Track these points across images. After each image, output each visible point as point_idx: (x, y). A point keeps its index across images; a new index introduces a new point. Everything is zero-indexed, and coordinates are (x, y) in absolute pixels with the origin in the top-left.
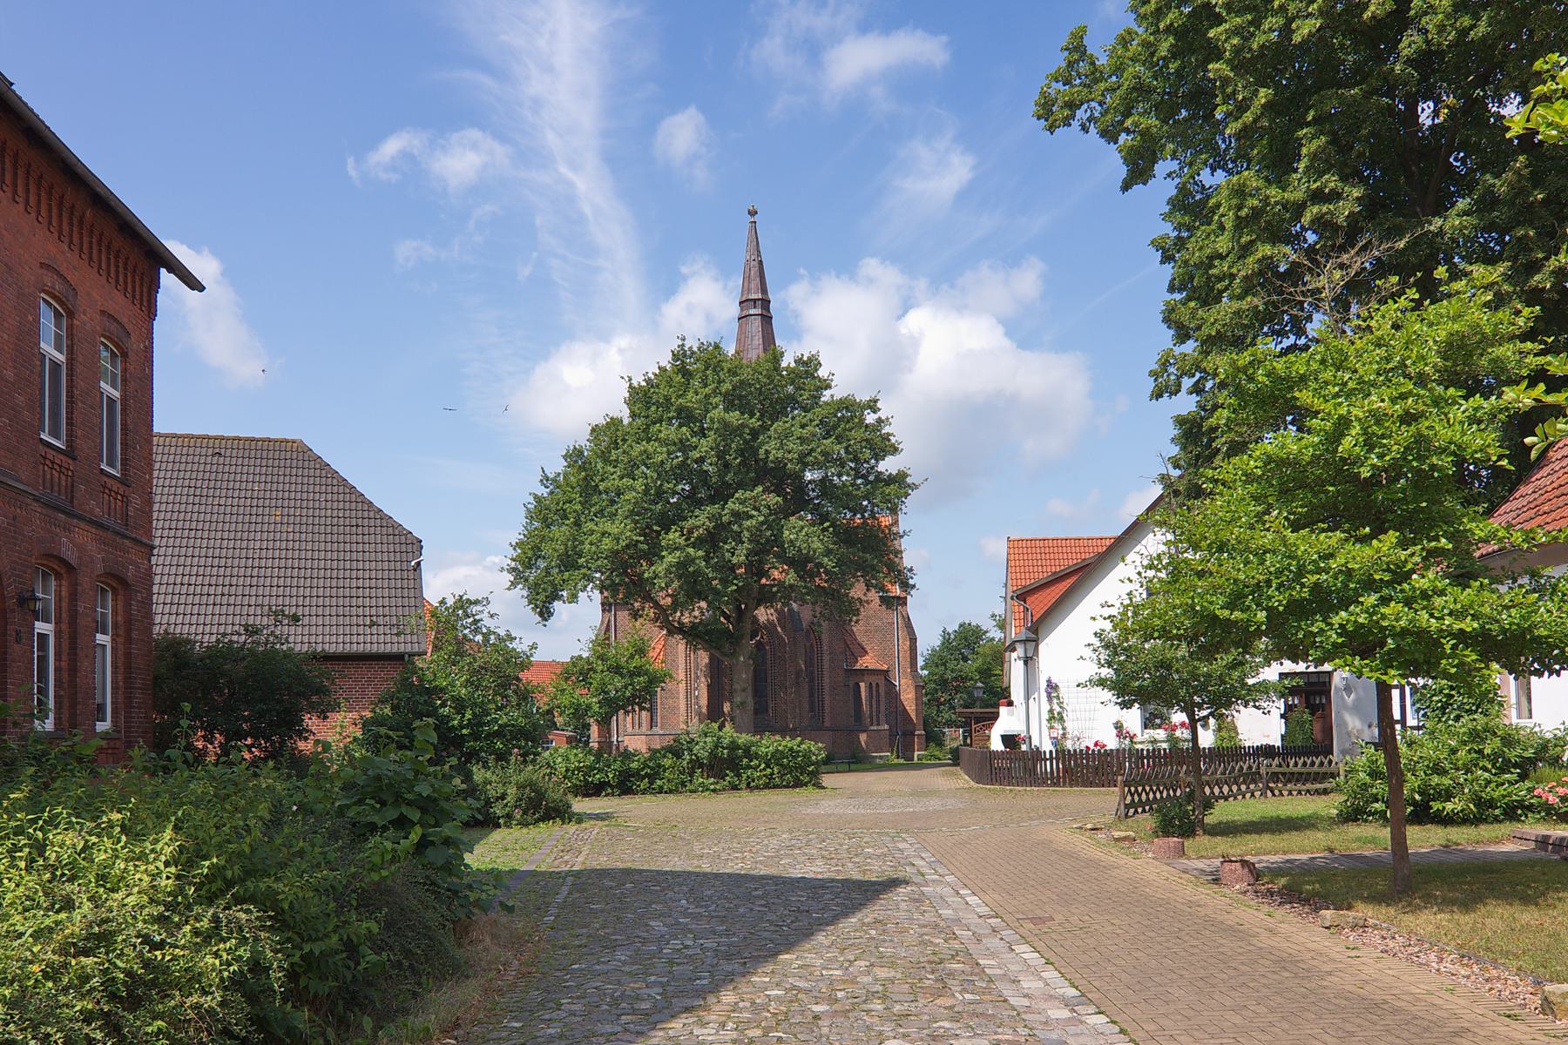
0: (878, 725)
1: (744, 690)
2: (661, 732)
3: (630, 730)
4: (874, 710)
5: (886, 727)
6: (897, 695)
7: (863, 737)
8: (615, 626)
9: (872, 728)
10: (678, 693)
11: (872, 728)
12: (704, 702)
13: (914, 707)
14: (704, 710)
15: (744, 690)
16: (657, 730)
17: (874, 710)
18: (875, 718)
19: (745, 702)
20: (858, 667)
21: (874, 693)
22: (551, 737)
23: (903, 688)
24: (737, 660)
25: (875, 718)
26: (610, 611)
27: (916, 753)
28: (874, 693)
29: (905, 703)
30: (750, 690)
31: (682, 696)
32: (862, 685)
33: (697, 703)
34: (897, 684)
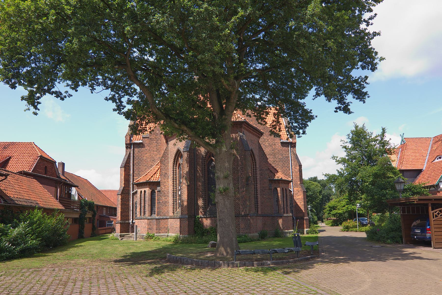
0: (287, 213)
1: (226, 178)
2: (157, 217)
3: (138, 216)
4: (285, 204)
5: (291, 214)
6: (292, 197)
7: (280, 221)
8: (133, 156)
9: (285, 215)
10: (168, 193)
11: (285, 215)
12: (185, 197)
13: (303, 203)
14: (185, 204)
15: (226, 178)
16: (155, 216)
17: (285, 204)
18: (285, 209)
19: (227, 189)
20: (276, 178)
21: (285, 194)
22: (111, 220)
23: (295, 193)
24: (220, 150)
25: (285, 209)
26: (130, 148)
27: (305, 230)
28: (285, 194)
29: (297, 201)
30: (231, 178)
31: (171, 195)
32: (279, 189)
33: (180, 199)
34: (292, 190)
